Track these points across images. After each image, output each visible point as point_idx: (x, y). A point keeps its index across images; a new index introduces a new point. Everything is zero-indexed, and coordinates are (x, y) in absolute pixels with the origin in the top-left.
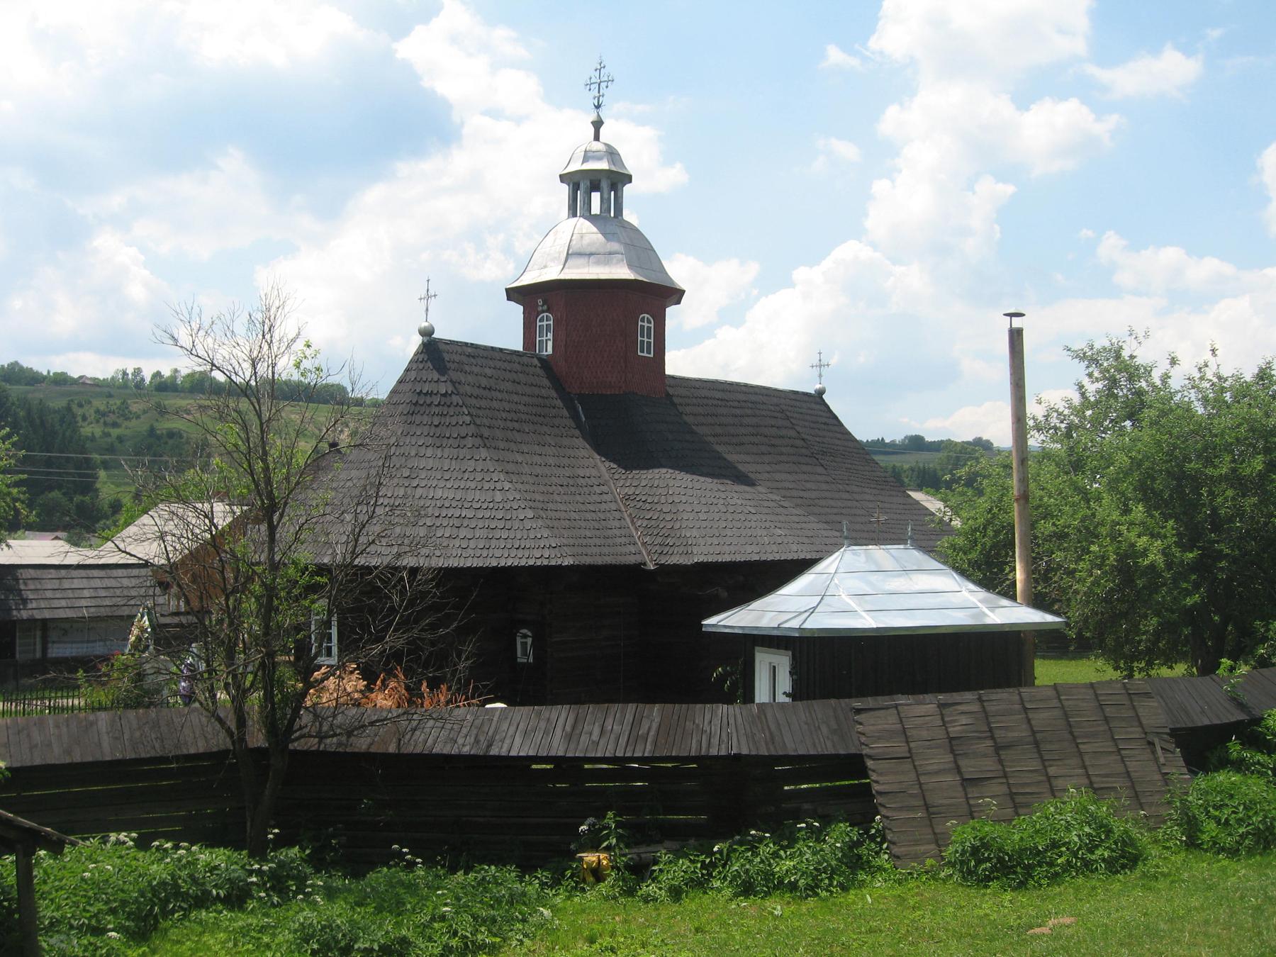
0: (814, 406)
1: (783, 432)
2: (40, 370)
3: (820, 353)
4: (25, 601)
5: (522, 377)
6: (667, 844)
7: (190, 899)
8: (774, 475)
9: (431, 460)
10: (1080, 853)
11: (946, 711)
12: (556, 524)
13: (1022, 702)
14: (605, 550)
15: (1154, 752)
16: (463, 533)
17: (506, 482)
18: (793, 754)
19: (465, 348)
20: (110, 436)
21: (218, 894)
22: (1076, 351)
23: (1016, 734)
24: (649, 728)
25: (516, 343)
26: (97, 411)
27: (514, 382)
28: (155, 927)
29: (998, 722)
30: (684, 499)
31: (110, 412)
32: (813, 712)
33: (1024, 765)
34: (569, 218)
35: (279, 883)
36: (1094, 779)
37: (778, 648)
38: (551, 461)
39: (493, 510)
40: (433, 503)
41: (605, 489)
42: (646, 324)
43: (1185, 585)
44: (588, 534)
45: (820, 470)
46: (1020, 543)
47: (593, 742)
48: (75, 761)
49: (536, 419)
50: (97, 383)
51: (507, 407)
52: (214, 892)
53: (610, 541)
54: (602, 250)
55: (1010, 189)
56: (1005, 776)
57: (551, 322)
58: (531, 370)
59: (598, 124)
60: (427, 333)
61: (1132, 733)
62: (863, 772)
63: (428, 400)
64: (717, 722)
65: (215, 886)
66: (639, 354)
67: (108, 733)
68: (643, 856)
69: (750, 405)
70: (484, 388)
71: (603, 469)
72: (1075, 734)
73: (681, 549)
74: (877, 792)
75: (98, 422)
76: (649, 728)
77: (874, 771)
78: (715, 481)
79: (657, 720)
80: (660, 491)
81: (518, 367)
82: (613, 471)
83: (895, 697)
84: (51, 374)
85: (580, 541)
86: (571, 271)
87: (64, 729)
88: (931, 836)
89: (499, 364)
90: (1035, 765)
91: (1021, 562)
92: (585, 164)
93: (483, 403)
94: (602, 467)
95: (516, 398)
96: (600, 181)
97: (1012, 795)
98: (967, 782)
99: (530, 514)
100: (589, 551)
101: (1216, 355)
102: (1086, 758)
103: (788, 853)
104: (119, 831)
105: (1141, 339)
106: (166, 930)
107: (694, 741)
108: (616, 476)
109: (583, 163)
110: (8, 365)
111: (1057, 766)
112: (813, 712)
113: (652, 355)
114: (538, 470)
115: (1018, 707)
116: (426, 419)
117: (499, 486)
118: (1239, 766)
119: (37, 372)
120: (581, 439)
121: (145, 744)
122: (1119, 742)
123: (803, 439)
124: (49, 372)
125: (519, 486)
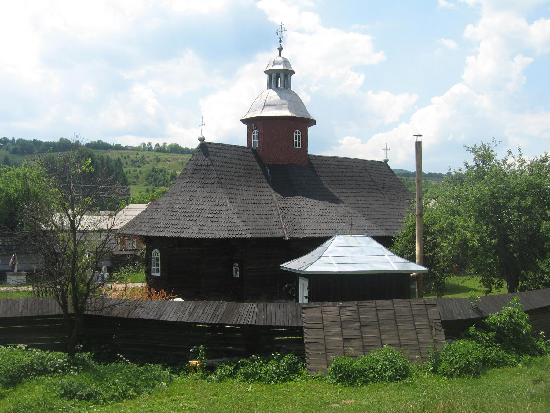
0: (382, 167)
1: (365, 179)
2: (110, 144)
3: (386, 144)
9: (199, 193)
10: (380, 373)
12: (247, 220)
13: (376, 307)
14: (267, 231)
15: (431, 330)
16: (208, 223)
19: (218, 146)
20: (136, 171)
21: (50, 370)
23: (370, 320)
25: (244, 143)
26: (132, 161)
29: (363, 315)
30: (305, 210)
31: (137, 161)
32: (287, 308)
33: (372, 333)
34: (268, 89)
36: (402, 341)
37: (305, 278)
38: (251, 193)
39: (221, 214)
40: (198, 211)
42: (298, 134)
43: (489, 254)
44: (261, 224)
45: (381, 195)
46: (418, 235)
48: (7, 316)
49: (247, 175)
50: (133, 149)
51: (234, 170)
53: (271, 227)
54: (279, 103)
55: (531, 60)
57: (258, 134)
59: (280, 49)
60: (202, 140)
61: (423, 322)
62: (302, 333)
63: (200, 168)
64: (246, 310)
65: (51, 367)
66: (294, 147)
68: (214, 363)
69: (350, 167)
70: (225, 163)
71: (274, 196)
72: (397, 321)
74: (305, 342)
75: (132, 165)
76: (221, 312)
77: (306, 333)
78: (321, 202)
81: (242, 153)
82: (278, 197)
83: (324, 302)
84: (115, 145)
86: (265, 112)
88: (325, 362)
89: (233, 152)
90: (377, 334)
91: (418, 243)
93: (224, 169)
94: (274, 195)
95: (239, 166)
96: (280, 73)
97: (363, 346)
98: (345, 340)
99: (236, 216)
101: (520, 151)
102: (400, 332)
104: (21, 343)
107: (236, 317)
111: (386, 334)
112: (287, 308)
113: (300, 148)
114: (244, 197)
116: (199, 176)
117: (225, 204)
118: (472, 337)
120: (267, 183)
121: (36, 310)
122: (416, 325)
123: (374, 182)
124: (113, 144)
125: (234, 204)
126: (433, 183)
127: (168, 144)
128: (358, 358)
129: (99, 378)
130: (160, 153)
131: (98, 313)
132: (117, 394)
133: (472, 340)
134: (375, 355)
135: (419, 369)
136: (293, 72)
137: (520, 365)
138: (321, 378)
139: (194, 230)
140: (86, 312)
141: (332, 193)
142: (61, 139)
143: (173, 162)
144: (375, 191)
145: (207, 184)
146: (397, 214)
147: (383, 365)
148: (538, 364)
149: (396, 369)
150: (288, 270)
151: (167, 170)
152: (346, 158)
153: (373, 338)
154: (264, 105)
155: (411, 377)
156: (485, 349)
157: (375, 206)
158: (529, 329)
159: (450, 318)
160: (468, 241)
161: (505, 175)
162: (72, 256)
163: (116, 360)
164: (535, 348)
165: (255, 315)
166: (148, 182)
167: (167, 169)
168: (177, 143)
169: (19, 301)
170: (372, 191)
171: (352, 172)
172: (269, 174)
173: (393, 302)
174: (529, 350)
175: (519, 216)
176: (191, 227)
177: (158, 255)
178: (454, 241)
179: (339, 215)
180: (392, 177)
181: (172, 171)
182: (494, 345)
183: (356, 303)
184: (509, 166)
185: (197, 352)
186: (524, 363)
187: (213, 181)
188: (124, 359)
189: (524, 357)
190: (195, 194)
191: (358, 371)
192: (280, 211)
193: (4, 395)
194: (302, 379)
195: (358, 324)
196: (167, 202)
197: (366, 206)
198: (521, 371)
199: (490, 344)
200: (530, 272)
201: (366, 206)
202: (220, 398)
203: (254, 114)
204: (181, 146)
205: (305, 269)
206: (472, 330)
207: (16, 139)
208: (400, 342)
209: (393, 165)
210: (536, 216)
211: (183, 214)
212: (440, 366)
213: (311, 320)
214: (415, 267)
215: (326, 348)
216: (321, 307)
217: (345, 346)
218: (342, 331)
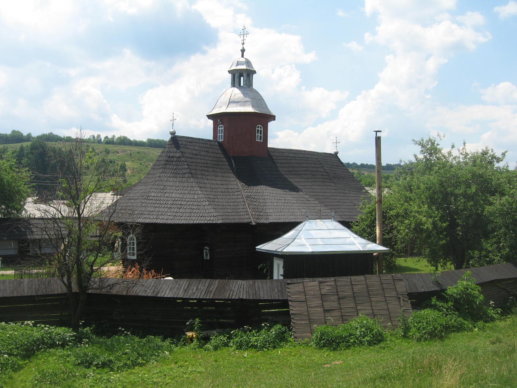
1: (319, 169)
2: (61, 136)
3: (336, 138)
4: (32, 232)
5: (210, 150)
6: (218, 330)
7: (48, 345)
8: (312, 187)
11: (321, 285)
12: (217, 207)
13: (351, 282)
14: (236, 217)
15: (400, 301)
16: (181, 210)
17: (199, 191)
18: (262, 299)
19: (188, 139)
21: (59, 343)
22: (417, 142)
23: (347, 294)
24: (213, 288)
25: (211, 137)
27: (207, 152)
28: (34, 354)
32: (273, 284)
35: (78, 340)
36: (375, 311)
37: (280, 258)
38: (219, 182)
39: (194, 202)
40: (171, 199)
41: (239, 193)
42: (259, 129)
43: (441, 236)
44: (230, 211)
45: (333, 184)
46: (378, 219)
47: (193, 293)
49: (214, 166)
51: (203, 162)
52: (57, 343)
53: (238, 214)
54: (242, 101)
56: (340, 309)
57: (223, 128)
58: (215, 147)
59: (243, 51)
62: (287, 306)
64: (237, 286)
65: (59, 340)
66: (257, 140)
67: (27, 286)
68: (208, 334)
69: (305, 159)
70: (194, 155)
71: (240, 185)
72: (370, 294)
73: (265, 217)
76: (213, 288)
77: (291, 306)
78: (282, 190)
79: (217, 285)
80: (260, 194)
81: (209, 146)
83: (305, 279)
84: (65, 137)
85: (226, 214)
87: (12, 284)
88: (310, 330)
89: (201, 145)
90: (353, 305)
91: (378, 226)
92: (237, 67)
93: (193, 160)
94: (240, 185)
95: (207, 158)
96: (243, 73)
97: (342, 316)
98: (326, 311)
99: (207, 203)
100: (229, 218)
102: (373, 303)
103: (257, 335)
104: (28, 320)
105: (441, 138)
106: (37, 355)
107: (228, 293)
108: (244, 188)
109: (236, 66)
110: (48, 134)
113: (262, 141)
114: (213, 186)
115: (349, 283)
116: (171, 167)
117: (196, 192)
118: (434, 307)
119: (60, 137)
120: (232, 173)
123: (327, 172)
124: (64, 136)
125: (204, 192)
126: (366, 174)
127: (117, 136)
128: (338, 327)
129: (111, 349)
130: (109, 145)
131: (98, 291)
132: (128, 362)
133: (434, 309)
134: (354, 324)
135: (391, 335)
136: (255, 72)
137: (476, 329)
138: (307, 344)
139: (169, 216)
140: (90, 291)
141: (291, 182)
142: (14, 132)
143: (122, 154)
144: (328, 180)
145: (179, 174)
146: (347, 201)
147: (361, 332)
148: (491, 328)
149: (373, 334)
150: (265, 251)
151: (116, 161)
152: (301, 151)
153: (350, 309)
154: (229, 102)
155: (386, 341)
156: (446, 317)
157: (328, 194)
158: (482, 299)
159: (414, 290)
160: (423, 224)
161: (451, 166)
162: (77, 240)
163: (117, 333)
164: (486, 316)
165: (245, 290)
166: (98, 172)
167: (116, 160)
168: (125, 136)
169: (24, 281)
170: (325, 180)
171: (307, 163)
172: (234, 165)
173: (365, 277)
174: (482, 318)
175: (465, 202)
176: (166, 214)
177: (134, 240)
178: (410, 225)
179: (300, 202)
180: (342, 168)
181: (122, 162)
182: (453, 313)
183: (333, 279)
184: (455, 158)
185: (192, 325)
186: (479, 328)
187: (185, 171)
188: (125, 332)
189: (479, 323)
190: (168, 184)
191: (341, 337)
192: (246, 199)
193: (22, 366)
194: (290, 346)
195: (337, 297)
196: (142, 191)
197: (320, 194)
198: (478, 335)
199: (450, 312)
200: (476, 251)
201: (320, 194)
202: (222, 363)
203: (219, 110)
204: (129, 139)
205: (283, 250)
206: (434, 301)
207: (47, 134)
208: (373, 312)
209: (345, 158)
210: (479, 202)
211: (158, 202)
212: (410, 332)
213: (295, 294)
214: (376, 247)
215: (309, 319)
216: (303, 282)
217: (326, 316)
218: (322, 303)
